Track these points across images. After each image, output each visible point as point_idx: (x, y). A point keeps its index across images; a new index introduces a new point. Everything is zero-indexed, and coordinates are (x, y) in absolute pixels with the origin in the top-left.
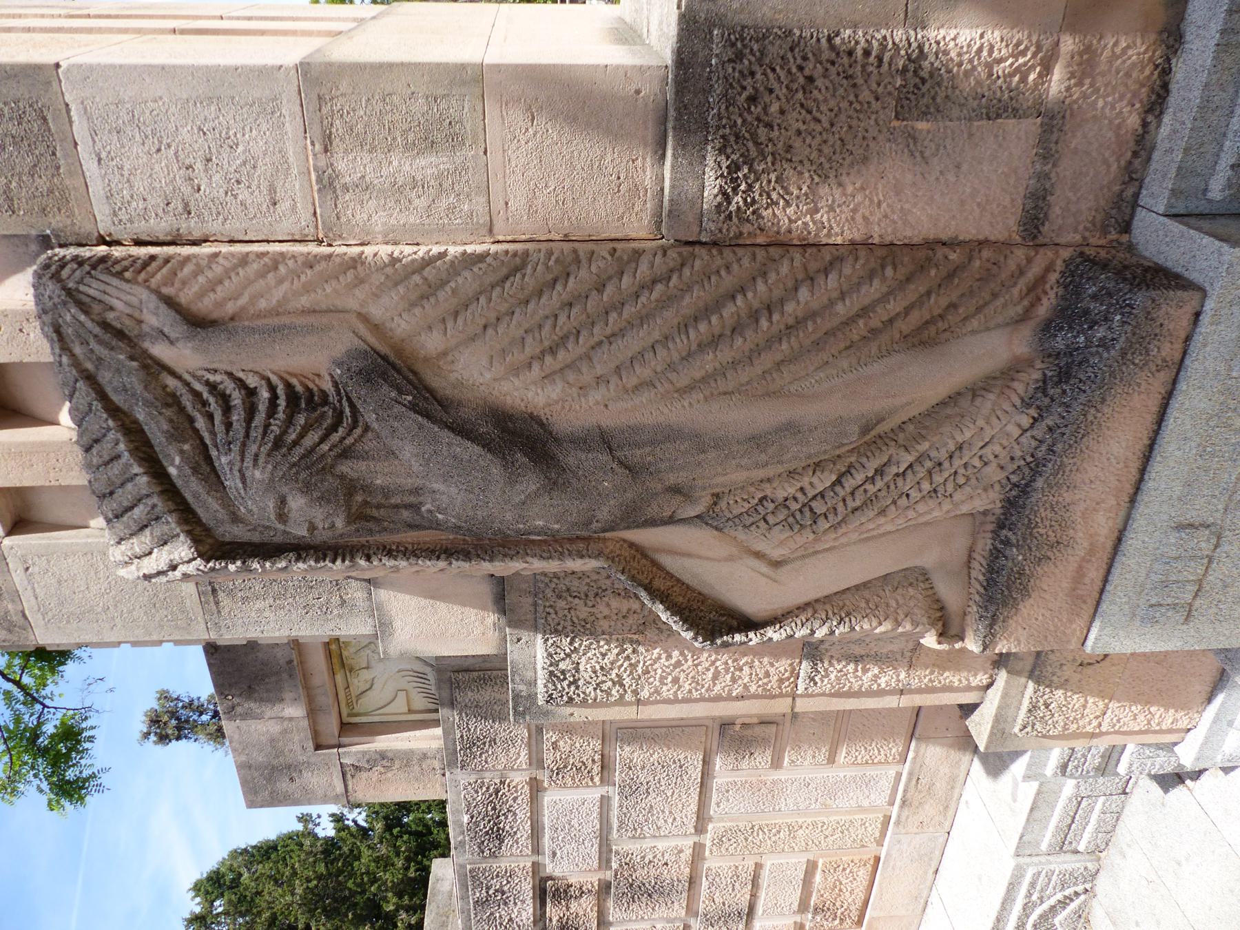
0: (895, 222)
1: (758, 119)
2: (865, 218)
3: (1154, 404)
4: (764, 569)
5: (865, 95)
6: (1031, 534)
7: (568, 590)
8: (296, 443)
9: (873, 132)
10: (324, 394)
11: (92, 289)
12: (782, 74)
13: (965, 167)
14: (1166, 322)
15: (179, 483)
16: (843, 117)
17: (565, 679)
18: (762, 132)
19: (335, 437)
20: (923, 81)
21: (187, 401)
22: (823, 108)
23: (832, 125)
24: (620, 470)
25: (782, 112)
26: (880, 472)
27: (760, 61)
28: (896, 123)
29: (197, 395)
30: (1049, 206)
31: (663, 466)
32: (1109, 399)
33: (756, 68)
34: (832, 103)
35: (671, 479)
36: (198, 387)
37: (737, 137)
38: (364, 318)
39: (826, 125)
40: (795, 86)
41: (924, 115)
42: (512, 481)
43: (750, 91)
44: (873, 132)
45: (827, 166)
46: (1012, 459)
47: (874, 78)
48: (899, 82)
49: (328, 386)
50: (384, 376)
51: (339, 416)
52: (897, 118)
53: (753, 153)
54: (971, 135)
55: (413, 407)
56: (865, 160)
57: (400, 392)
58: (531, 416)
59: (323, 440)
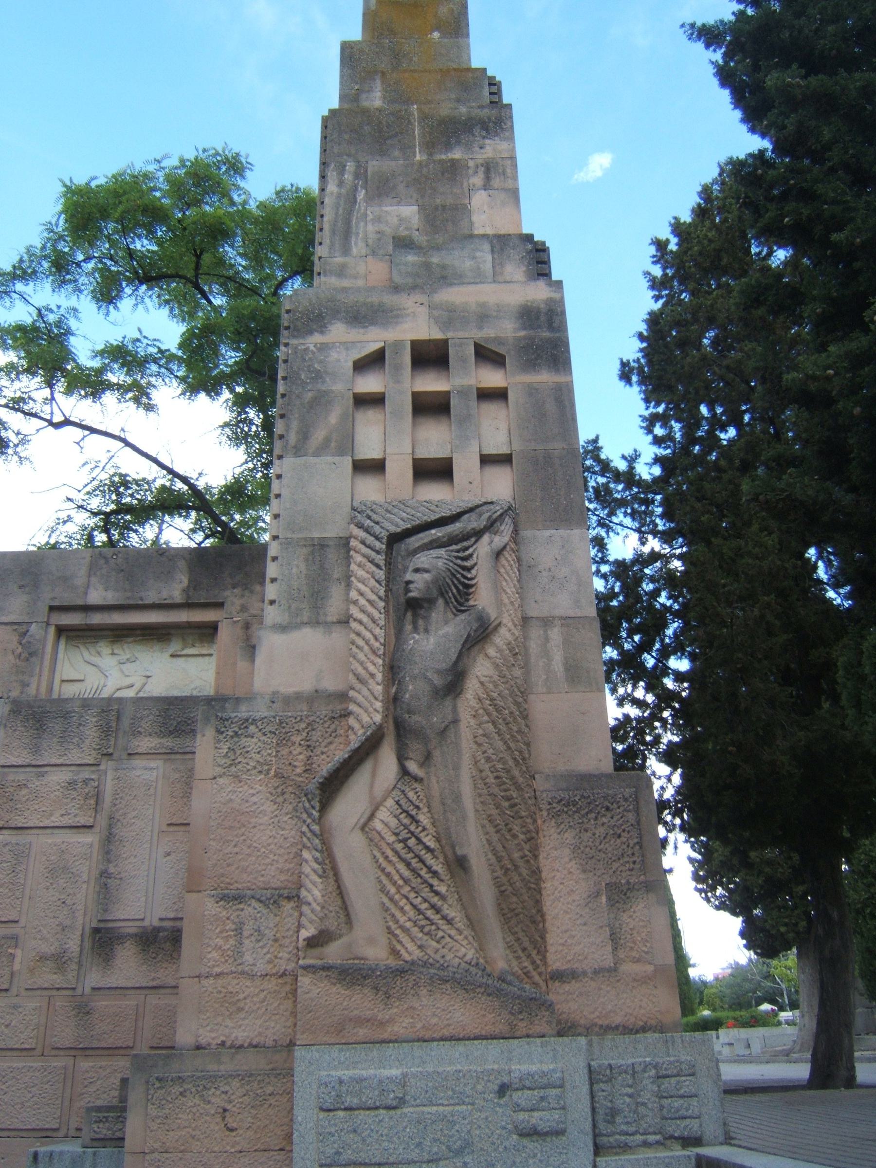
0: (553, 894)
1: (598, 813)
2: (554, 877)
3: (489, 1029)
4: (362, 821)
5: (615, 865)
6: (396, 976)
7: (313, 730)
8: (453, 582)
9: (599, 873)
10: (467, 600)
11: (507, 520)
12: (621, 822)
13: (584, 928)
14: (538, 1017)
15: (427, 533)
16: (604, 855)
17: (240, 729)
18: (593, 815)
19: (453, 600)
20: (625, 894)
21: (465, 544)
22: (607, 845)
23: (599, 851)
24: (443, 725)
25: (603, 824)
26: (435, 874)
27: (625, 810)
28: (603, 884)
29: (467, 548)
30: (569, 983)
31: (445, 749)
32: (491, 998)
33: (622, 808)
34: (610, 849)
35: (437, 754)
36: (471, 550)
37: (589, 803)
38: (499, 624)
39: (599, 848)
40: (616, 829)
41: (609, 899)
42: (439, 672)
43: (612, 807)
44: (599, 873)
45: (579, 851)
46: (443, 957)
47: (624, 868)
48: (623, 881)
49: (471, 603)
50: (481, 626)
51: (461, 604)
52: (607, 884)
53: (583, 812)
54: (601, 927)
55: (469, 635)
56: (584, 871)
57: (475, 631)
58: (462, 690)
59: (453, 594)
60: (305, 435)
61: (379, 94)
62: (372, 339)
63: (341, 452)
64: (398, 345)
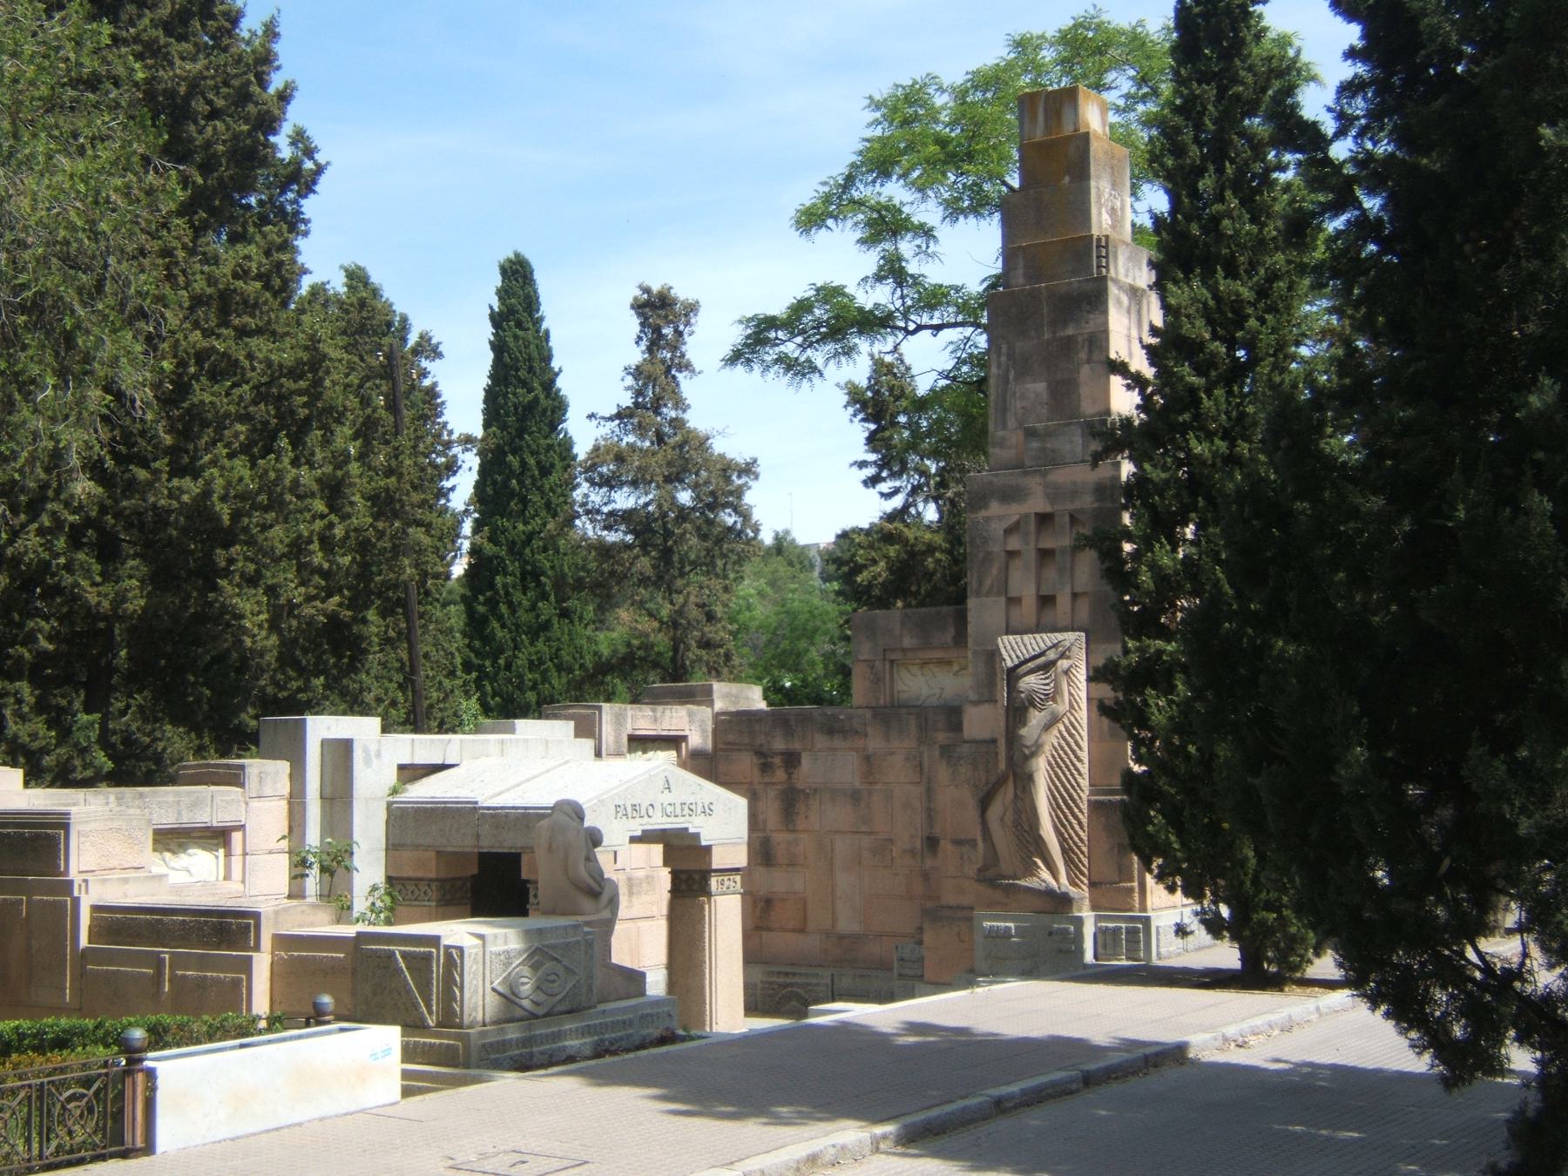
60: (980, 584)
61: (1021, 271)
62: (1014, 511)
63: (999, 594)
64: (1027, 516)
